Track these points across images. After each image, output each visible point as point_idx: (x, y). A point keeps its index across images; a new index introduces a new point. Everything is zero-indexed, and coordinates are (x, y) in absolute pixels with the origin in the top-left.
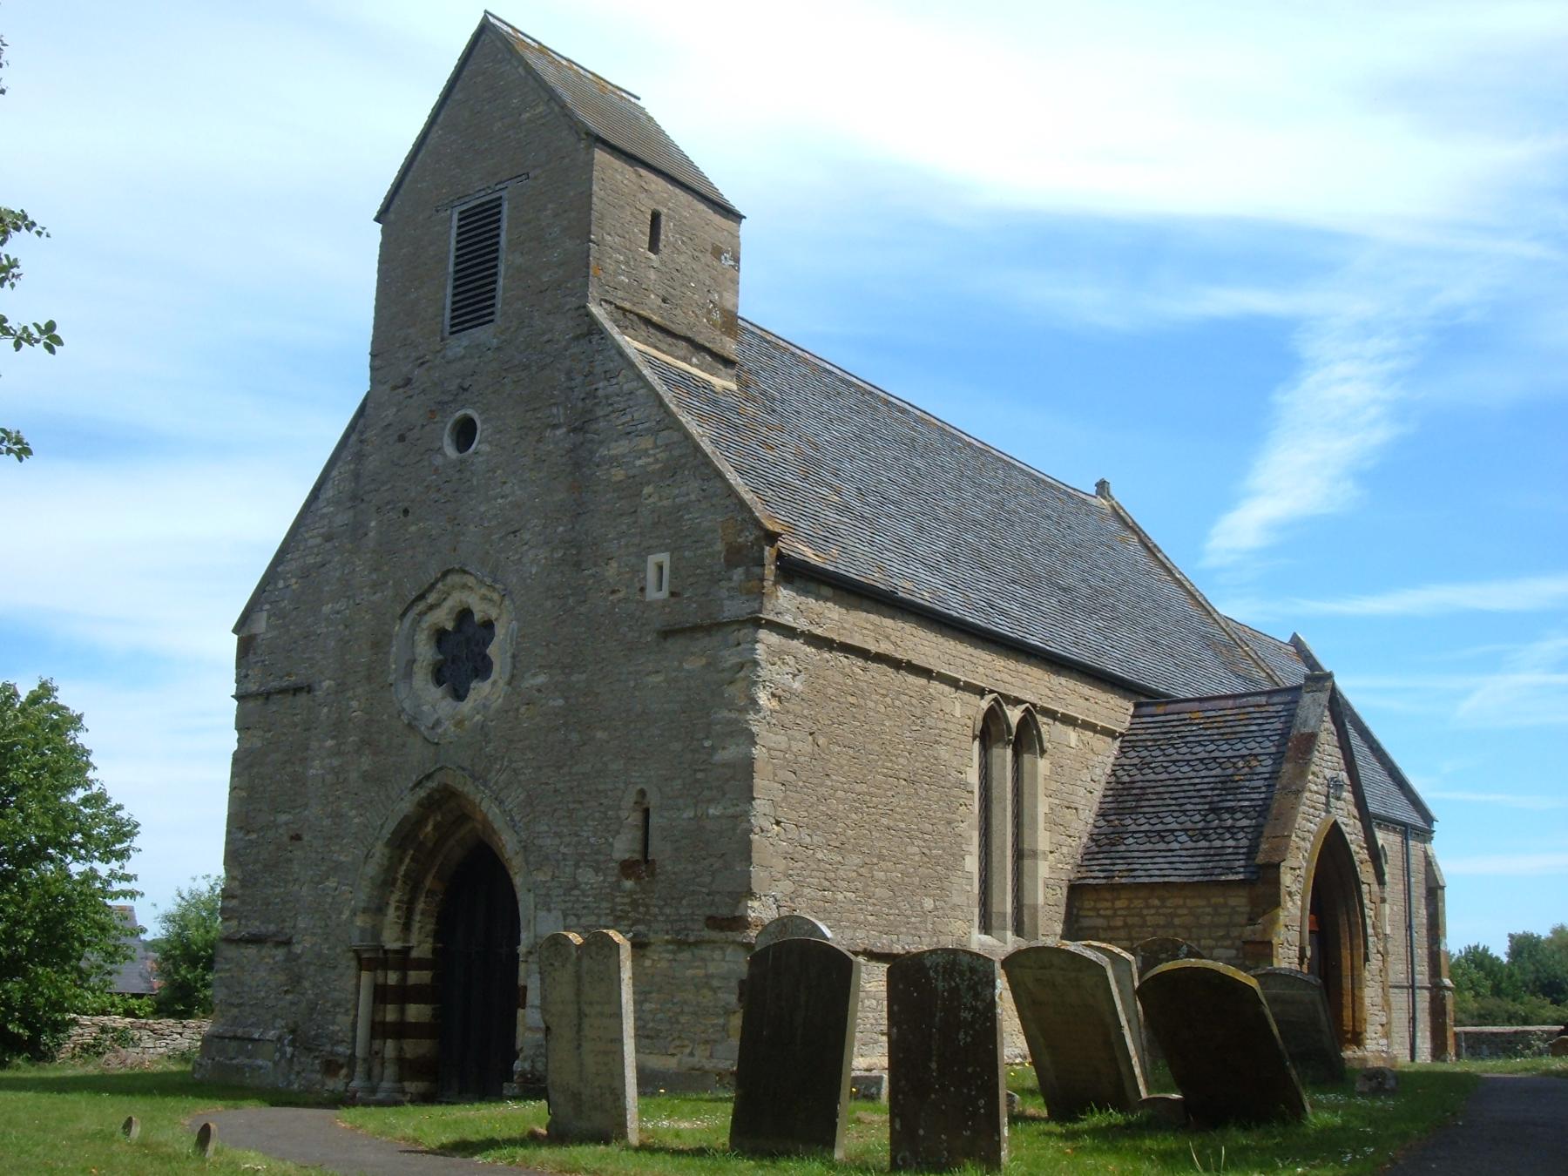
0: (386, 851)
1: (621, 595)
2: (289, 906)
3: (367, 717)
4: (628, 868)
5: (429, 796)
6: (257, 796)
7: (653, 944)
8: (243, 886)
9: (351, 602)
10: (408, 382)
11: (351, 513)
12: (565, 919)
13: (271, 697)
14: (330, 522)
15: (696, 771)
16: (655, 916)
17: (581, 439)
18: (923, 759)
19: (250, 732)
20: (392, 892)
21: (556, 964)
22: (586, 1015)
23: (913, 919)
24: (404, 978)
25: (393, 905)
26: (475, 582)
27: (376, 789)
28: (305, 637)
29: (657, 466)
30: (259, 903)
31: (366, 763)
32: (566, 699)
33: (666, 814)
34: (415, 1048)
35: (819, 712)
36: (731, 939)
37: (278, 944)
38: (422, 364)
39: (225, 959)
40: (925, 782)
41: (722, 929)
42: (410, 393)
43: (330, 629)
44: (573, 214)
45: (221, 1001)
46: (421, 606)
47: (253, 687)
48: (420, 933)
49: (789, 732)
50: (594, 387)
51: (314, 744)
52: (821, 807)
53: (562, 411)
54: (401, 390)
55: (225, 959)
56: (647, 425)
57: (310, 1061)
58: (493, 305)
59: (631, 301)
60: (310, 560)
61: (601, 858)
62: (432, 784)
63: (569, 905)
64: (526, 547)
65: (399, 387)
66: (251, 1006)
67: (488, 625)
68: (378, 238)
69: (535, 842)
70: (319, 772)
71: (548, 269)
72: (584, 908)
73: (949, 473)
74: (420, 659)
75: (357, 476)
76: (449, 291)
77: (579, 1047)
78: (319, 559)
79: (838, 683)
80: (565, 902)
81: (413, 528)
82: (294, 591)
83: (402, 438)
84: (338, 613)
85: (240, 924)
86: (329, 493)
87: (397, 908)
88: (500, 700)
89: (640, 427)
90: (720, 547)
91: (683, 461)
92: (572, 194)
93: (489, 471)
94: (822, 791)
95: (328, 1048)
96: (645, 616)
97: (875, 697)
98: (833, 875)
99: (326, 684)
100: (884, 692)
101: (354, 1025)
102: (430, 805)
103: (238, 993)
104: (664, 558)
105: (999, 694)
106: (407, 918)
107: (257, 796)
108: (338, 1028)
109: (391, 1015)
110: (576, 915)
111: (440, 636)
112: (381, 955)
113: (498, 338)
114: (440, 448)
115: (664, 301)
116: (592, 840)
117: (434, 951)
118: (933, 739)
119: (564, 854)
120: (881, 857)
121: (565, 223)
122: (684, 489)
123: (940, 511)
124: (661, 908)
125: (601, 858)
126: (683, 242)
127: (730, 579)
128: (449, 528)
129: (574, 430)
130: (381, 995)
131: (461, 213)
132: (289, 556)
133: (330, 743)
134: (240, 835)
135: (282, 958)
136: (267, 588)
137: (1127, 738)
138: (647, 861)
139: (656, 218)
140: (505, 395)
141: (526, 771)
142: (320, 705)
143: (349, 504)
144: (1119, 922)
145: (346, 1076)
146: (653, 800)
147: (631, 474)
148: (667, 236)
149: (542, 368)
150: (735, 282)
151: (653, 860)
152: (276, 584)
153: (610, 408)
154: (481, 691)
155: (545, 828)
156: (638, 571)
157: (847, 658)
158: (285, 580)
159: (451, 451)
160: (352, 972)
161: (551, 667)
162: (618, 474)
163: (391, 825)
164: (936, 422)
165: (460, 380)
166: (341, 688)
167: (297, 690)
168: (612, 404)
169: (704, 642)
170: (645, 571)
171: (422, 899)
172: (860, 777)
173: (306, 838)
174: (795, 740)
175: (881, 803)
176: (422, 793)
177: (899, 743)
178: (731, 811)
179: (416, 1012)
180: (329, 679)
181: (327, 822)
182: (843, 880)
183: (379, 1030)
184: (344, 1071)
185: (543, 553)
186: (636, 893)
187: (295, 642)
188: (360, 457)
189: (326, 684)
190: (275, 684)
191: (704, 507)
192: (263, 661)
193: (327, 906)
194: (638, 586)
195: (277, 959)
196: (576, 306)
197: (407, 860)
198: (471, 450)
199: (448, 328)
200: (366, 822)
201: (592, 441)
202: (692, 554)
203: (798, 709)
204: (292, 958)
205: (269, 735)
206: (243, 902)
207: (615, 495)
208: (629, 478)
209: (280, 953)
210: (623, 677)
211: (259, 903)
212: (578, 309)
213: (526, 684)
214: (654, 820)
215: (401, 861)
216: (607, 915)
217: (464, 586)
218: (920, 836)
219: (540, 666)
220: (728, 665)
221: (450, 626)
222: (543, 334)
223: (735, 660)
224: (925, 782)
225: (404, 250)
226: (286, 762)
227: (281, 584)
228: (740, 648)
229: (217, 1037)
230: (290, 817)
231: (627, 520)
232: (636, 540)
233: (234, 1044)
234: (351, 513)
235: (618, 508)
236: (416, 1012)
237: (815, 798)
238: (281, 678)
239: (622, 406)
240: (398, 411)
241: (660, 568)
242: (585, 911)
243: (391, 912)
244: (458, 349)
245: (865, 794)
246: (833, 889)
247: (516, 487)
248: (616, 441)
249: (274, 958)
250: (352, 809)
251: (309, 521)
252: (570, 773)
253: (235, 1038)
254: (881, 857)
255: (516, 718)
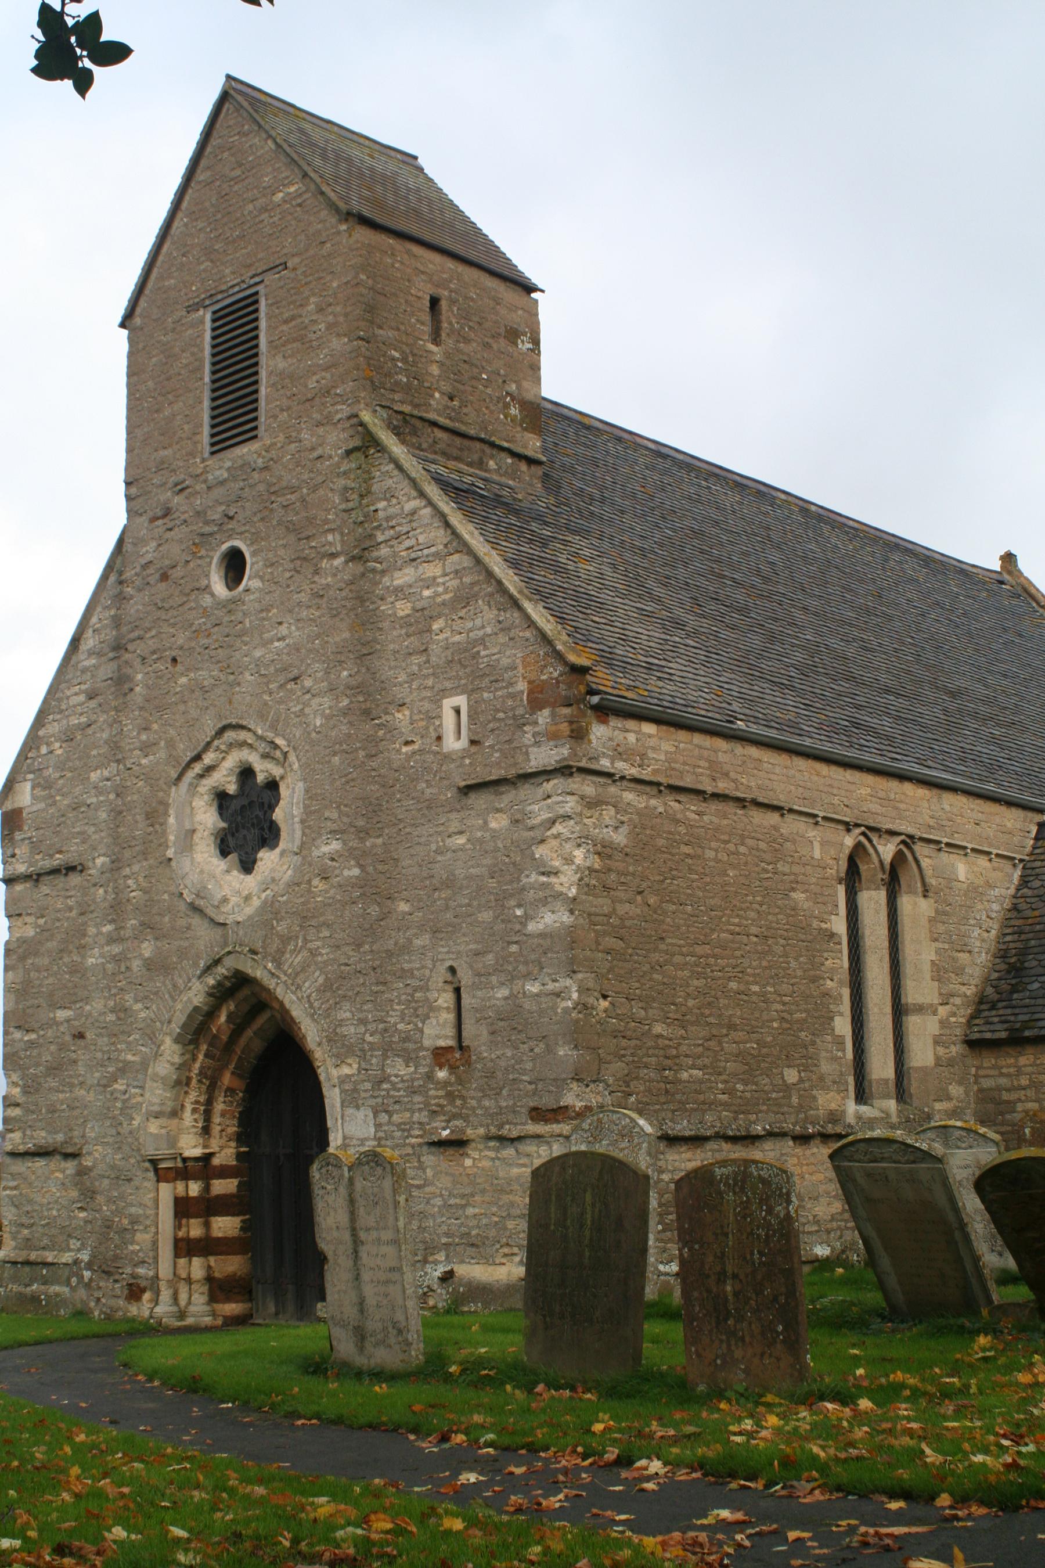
0: (177, 1048)
1: (416, 747)
2: (76, 1113)
3: (147, 897)
4: (440, 1055)
5: (220, 984)
6: (34, 990)
7: (473, 1140)
8: (26, 1092)
9: (121, 766)
10: (167, 513)
11: (114, 665)
12: (375, 1117)
13: (41, 879)
14: (93, 676)
15: (510, 943)
16: (473, 1109)
17: (362, 569)
18: (777, 910)
19: (20, 919)
20: (186, 1093)
21: (329, 1187)
22: (362, 1243)
23: (774, 1095)
24: (207, 1188)
25: (189, 1107)
26: (254, 738)
27: (161, 977)
28: (74, 809)
29: (447, 597)
30: (44, 1111)
31: (147, 949)
32: (361, 867)
33: (479, 993)
34: (231, 1265)
35: (648, 868)
36: (558, 1131)
37: (67, 1156)
38: (182, 490)
39: (11, 1174)
40: (781, 936)
41: (546, 1121)
42: (170, 525)
43: (102, 798)
44: (338, 309)
45: (10, 1221)
46: (198, 768)
47: (22, 869)
48: (221, 1137)
49: (612, 893)
50: (373, 508)
51: (92, 930)
52: (655, 976)
53: (338, 537)
54: (160, 522)
55: (11, 1174)
56: (433, 549)
57: (110, 1286)
58: (256, 419)
59: (411, 403)
60: (74, 721)
61: (411, 1046)
62: (221, 970)
63: (380, 1100)
64: (308, 696)
65: (158, 518)
66: (43, 1226)
67: (273, 785)
68: (124, 347)
69: (338, 1030)
70: (100, 960)
71: (315, 374)
72: (395, 1102)
73: (812, 564)
74: (200, 828)
75: (117, 622)
76: (206, 404)
77: (357, 1278)
78: (83, 719)
79: (670, 833)
80: (375, 1097)
81: (183, 680)
82: (58, 756)
83: (164, 577)
84: (108, 780)
85: (24, 1135)
86: (90, 642)
87: (194, 1111)
88: (290, 872)
89: (426, 552)
90: (522, 686)
91: (476, 589)
92: (335, 285)
93: (262, 611)
94: (655, 957)
95: (128, 1270)
96: (443, 768)
97: (713, 844)
98: (674, 1052)
99: (99, 861)
100: (725, 837)
101: (155, 1243)
102: (222, 994)
103: (28, 1212)
104: (461, 701)
105: (867, 827)
106: (205, 1121)
107: (34, 990)
108: (138, 1248)
109: (195, 1229)
110: (386, 1112)
111: (221, 798)
112: (180, 1164)
113: (263, 457)
114: (208, 586)
115: (451, 399)
116: (401, 1026)
117: (239, 1156)
118: (788, 886)
119: (370, 1043)
120: (732, 1027)
121: (331, 318)
122: (478, 622)
123: (799, 615)
124: (479, 1101)
125: (411, 1046)
126: (470, 328)
127: (536, 723)
128: (222, 677)
129: (353, 559)
130: (183, 1208)
131: (214, 313)
132: (51, 717)
133: (108, 928)
134: (17, 1035)
135: (73, 1172)
136: (30, 755)
137: (1029, 865)
138: (461, 1047)
139: (434, 302)
140: (275, 522)
141: (324, 952)
142: (95, 885)
143: (111, 655)
144: (1024, 1081)
145: (150, 1301)
146: (465, 977)
147: (419, 607)
148: (450, 323)
149: (315, 489)
150: (535, 368)
151: (468, 1047)
152: (38, 748)
153: (392, 532)
154: (267, 859)
155: (348, 1015)
156: (433, 717)
157: (679, 802)
158: (48, 744)
159: (219, 588)
160: (149, 1184)
161: (343, 832)
162: (403, 608)
163: (180, 1018)
164: (797, 501)
165: (224, 508)
166: (116, 864)
167: (71, 869)
168: (393, 527)
169: (508, 797)
170: (439, 717)
171: (221, 1099)
172: (702, 937)
173: (89, 1035)
174: (621, 901)
175: (727, 966)
176: (211, 981)
177: (747, 895)
178: (551, 986)
179: (225, 1226)
180: (104, 855)
181: (111, 1017)
182: (687, 1056)
183: (185, 1248)
184: (147, 1296)
185: (326, 701)
186: (451, 1085)
187: (63, 816)
188: (121, 598)
189: (99, 861)
190: (48, 864)
191: (502, 641)
192: (30, 838)
193: (117, 1112)
194: (434, 735)
195: (68, 1172)
196: (348, 414)
197: (201, 1057)
198: (241, 587)
199: (208, 447)
200: (152, 1016)
201: (374, 570)
202: (491, 696)
203: (620, 866)
204: (82, 1172)
205: (41, 921)
206: (28, 1111)
207: (404, 631)
208: (417, 611)
209: (70, 1166)
210: (423, 840)
211: (44, 1111)
212: (349, 418)
213: (316, 853)
214: (466, 1000)
215: (194, 1059)
216: (420, 1110)
217: (244, 744)
218: (778, 999)
219: (330, 832)
220: (536, 821)
221: (232, 789)
222: (313, 449)
223: (546, 815)
224: (781, 936)
225: (154, 360)
226: (61, 951)
227: (44, 750)
228: (549, 801)
229: (8, 1262)
230: (70, 1013)
231: (416, 660)
232: (430, 682)
233: (27, 1269)
234: (114, 665)
235: (407, 647)
236: (225, 1226)
237: (648, 966)
238: (51, 856)
239: (405, 529)
240: (160, 545)
241: (458, 711)
242: (397, 1107)
243: (188, 1116)
244: (218, 473)
245: (707, 956)
246: (675, 1068)
247: (293, 628)
248: (400, 570)
249: (64, 1172)
250: (136, 1001)
251: (70, 676)
252: (372, 951)
253: (27, 1263)
254: (732, 1027)
255: (309, 891)
